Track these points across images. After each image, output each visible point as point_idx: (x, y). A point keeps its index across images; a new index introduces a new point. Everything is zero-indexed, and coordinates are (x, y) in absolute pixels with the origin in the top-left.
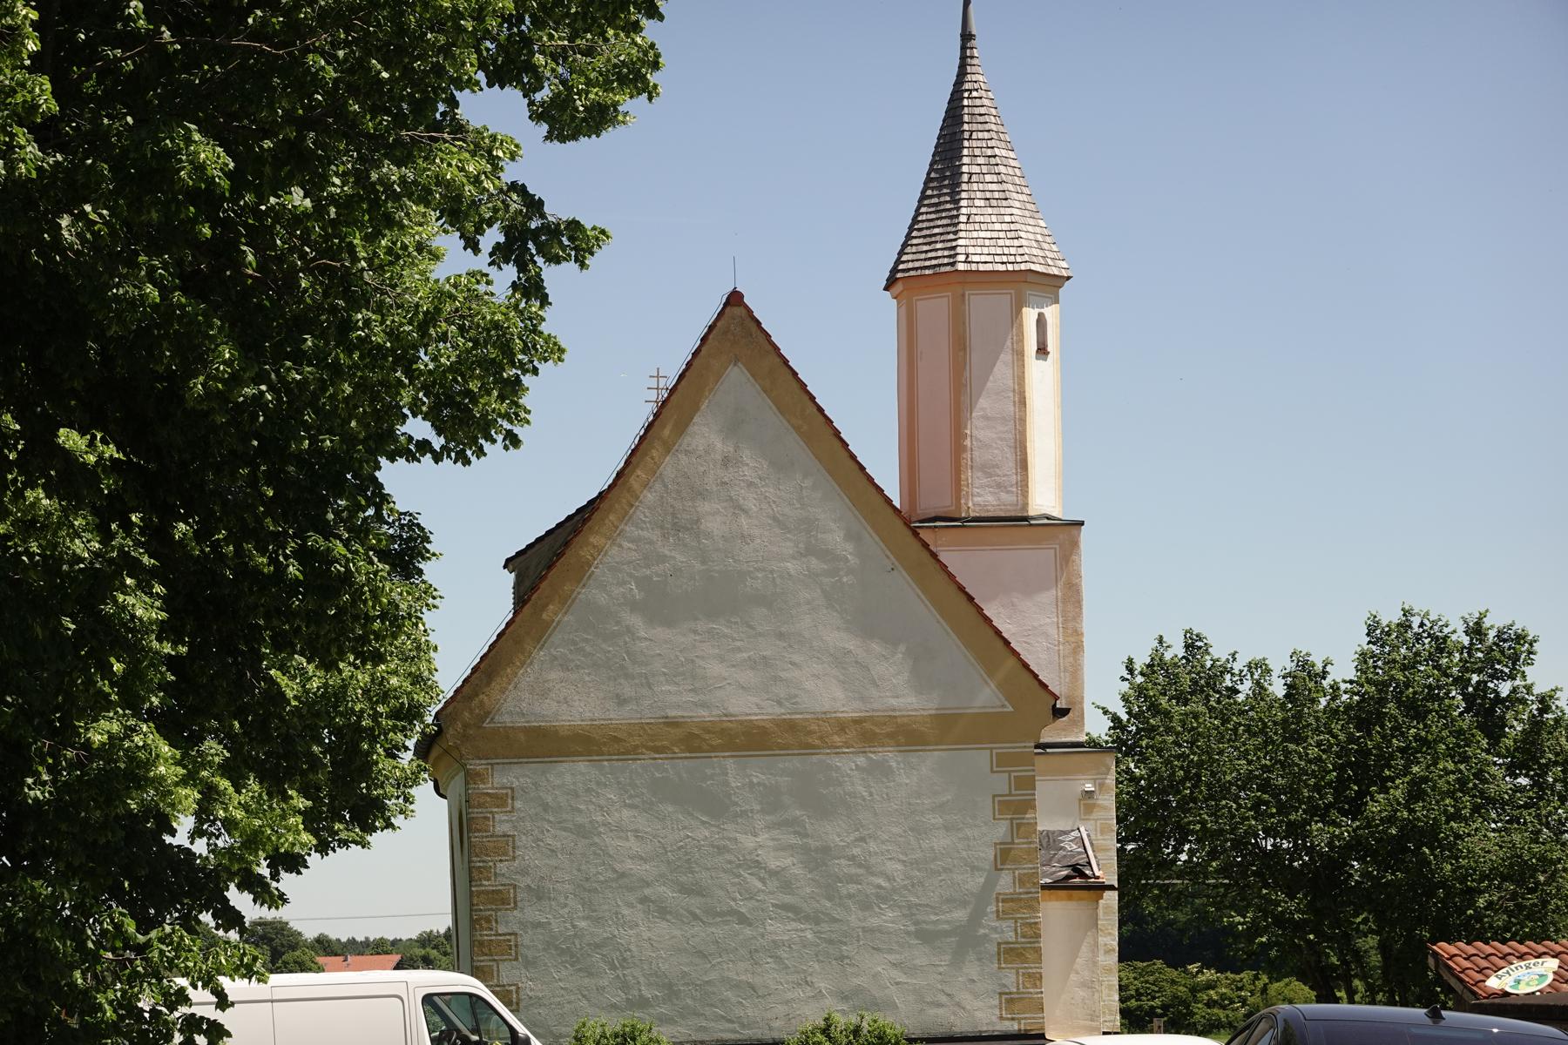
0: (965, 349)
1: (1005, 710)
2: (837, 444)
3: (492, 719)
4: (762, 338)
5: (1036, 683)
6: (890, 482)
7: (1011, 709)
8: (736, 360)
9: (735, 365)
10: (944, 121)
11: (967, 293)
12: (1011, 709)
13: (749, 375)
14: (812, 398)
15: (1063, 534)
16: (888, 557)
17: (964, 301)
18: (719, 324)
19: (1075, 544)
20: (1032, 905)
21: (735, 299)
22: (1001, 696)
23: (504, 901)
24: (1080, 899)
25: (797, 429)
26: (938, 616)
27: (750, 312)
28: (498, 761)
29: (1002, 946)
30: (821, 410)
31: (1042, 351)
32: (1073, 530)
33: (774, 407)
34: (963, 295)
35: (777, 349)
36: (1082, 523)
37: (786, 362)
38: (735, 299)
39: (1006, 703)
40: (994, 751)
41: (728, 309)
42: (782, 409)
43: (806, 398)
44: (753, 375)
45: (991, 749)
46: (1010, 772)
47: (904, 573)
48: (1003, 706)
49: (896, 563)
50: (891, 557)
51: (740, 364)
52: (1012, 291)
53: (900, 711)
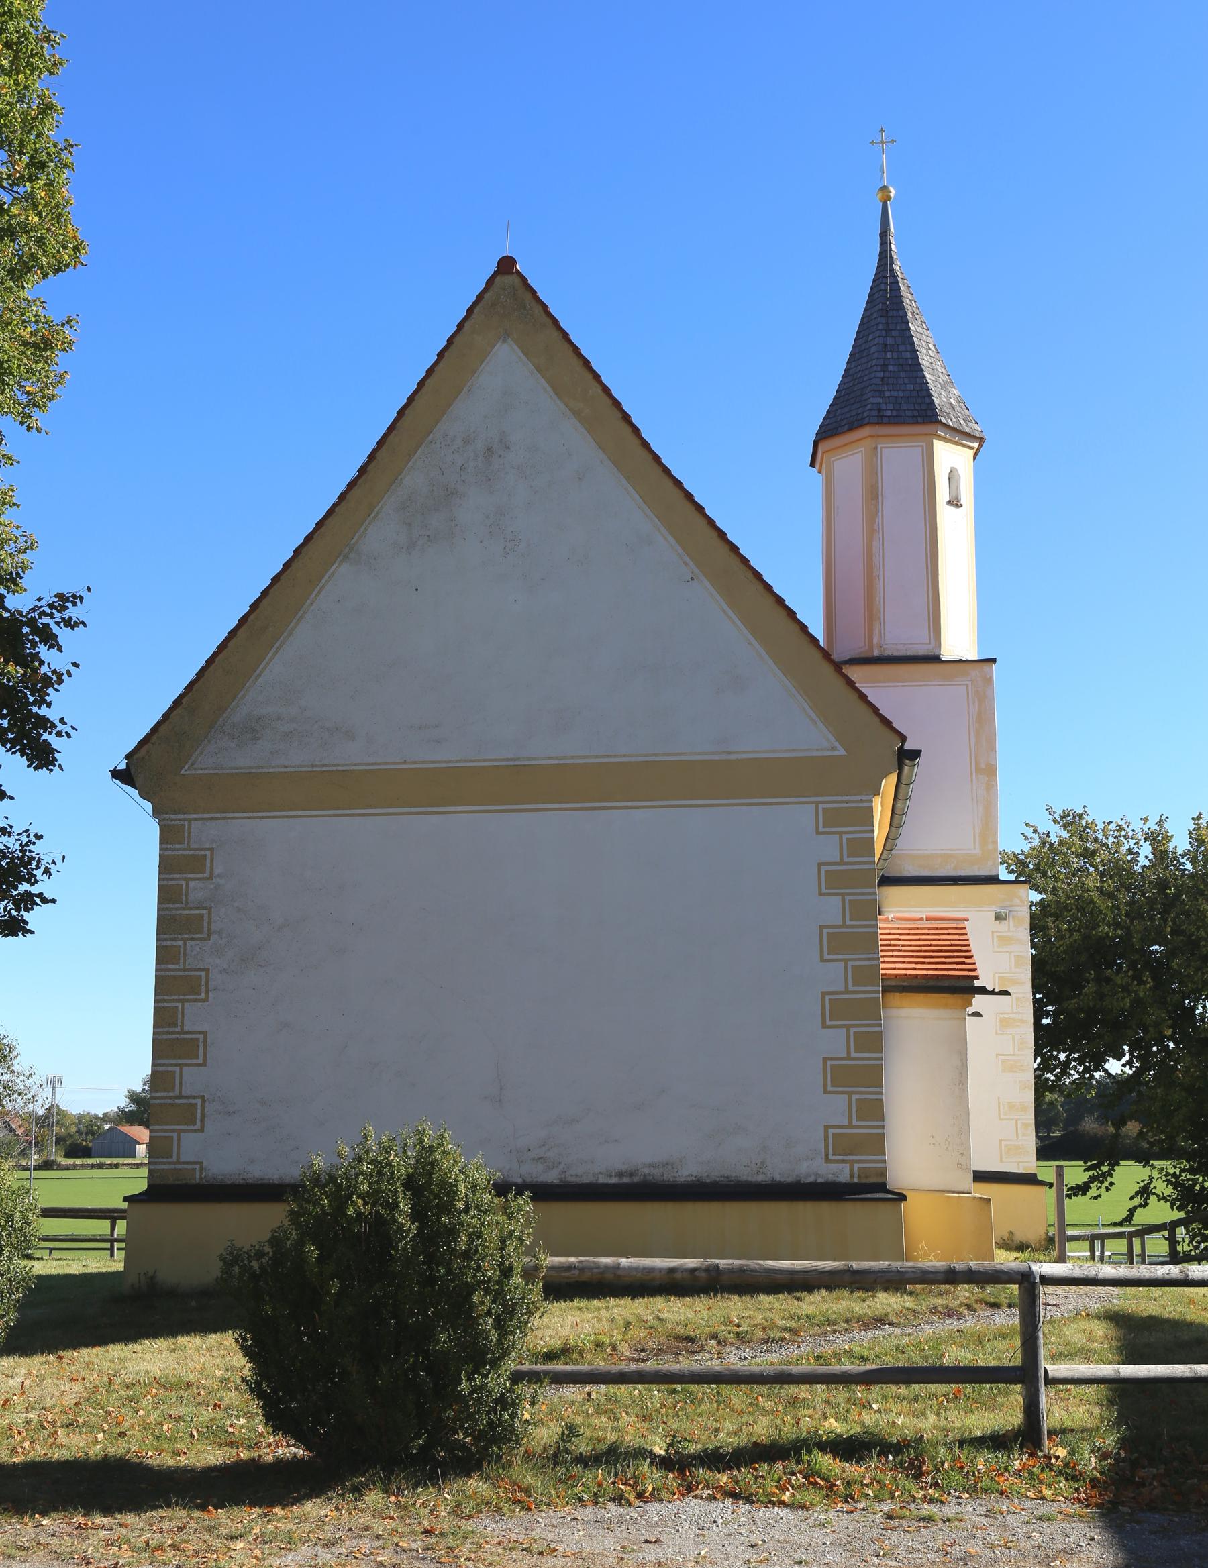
0: (878, 498)
1: (836, 753)
2: (627, 430)
3: (192, 764)
4: (538, 310)
5: (877, 719)
6: (817, 629)
7: (842, 752)
8: (506, 335)
9: (504, 341)
10: (862, 318)
11: (879, 446)
12: (842, 752)
13: (520, 353)
14: (597, 377)
15: (975, 672)
16: (686, 564)
17: (876, 455)
18: (486, 296)
19: (989, 681)
20: (872, 1011)
21: (506, 265)
22: (830, 736)
23: (194, 990)
24: (946, 1006)
25: (576, 413)
26: (750, 636)
27: (524, 280)
28: (195, 816)
29: (200, 1061)
30: (606, 390)
31: (955, 502)
32: (986, 667)
33: (549, 389)
34: (876, 448)
35: (555, 322)
36: (993, 660)
37: (565, 336)
38: (506, 265)
39: (837, 744)
40: (821, 806)
41: (498, 279)
42: (558, 390)
43: (590, 376)
44: (526, 354)
45: (817, 803)
46: (841, 833)
47: (706, 583)
48: (833, 748)
49: (697, 571)
50: (691, 563)
51: (510, 341)
52: (924, 444)
53: (369, 524)
